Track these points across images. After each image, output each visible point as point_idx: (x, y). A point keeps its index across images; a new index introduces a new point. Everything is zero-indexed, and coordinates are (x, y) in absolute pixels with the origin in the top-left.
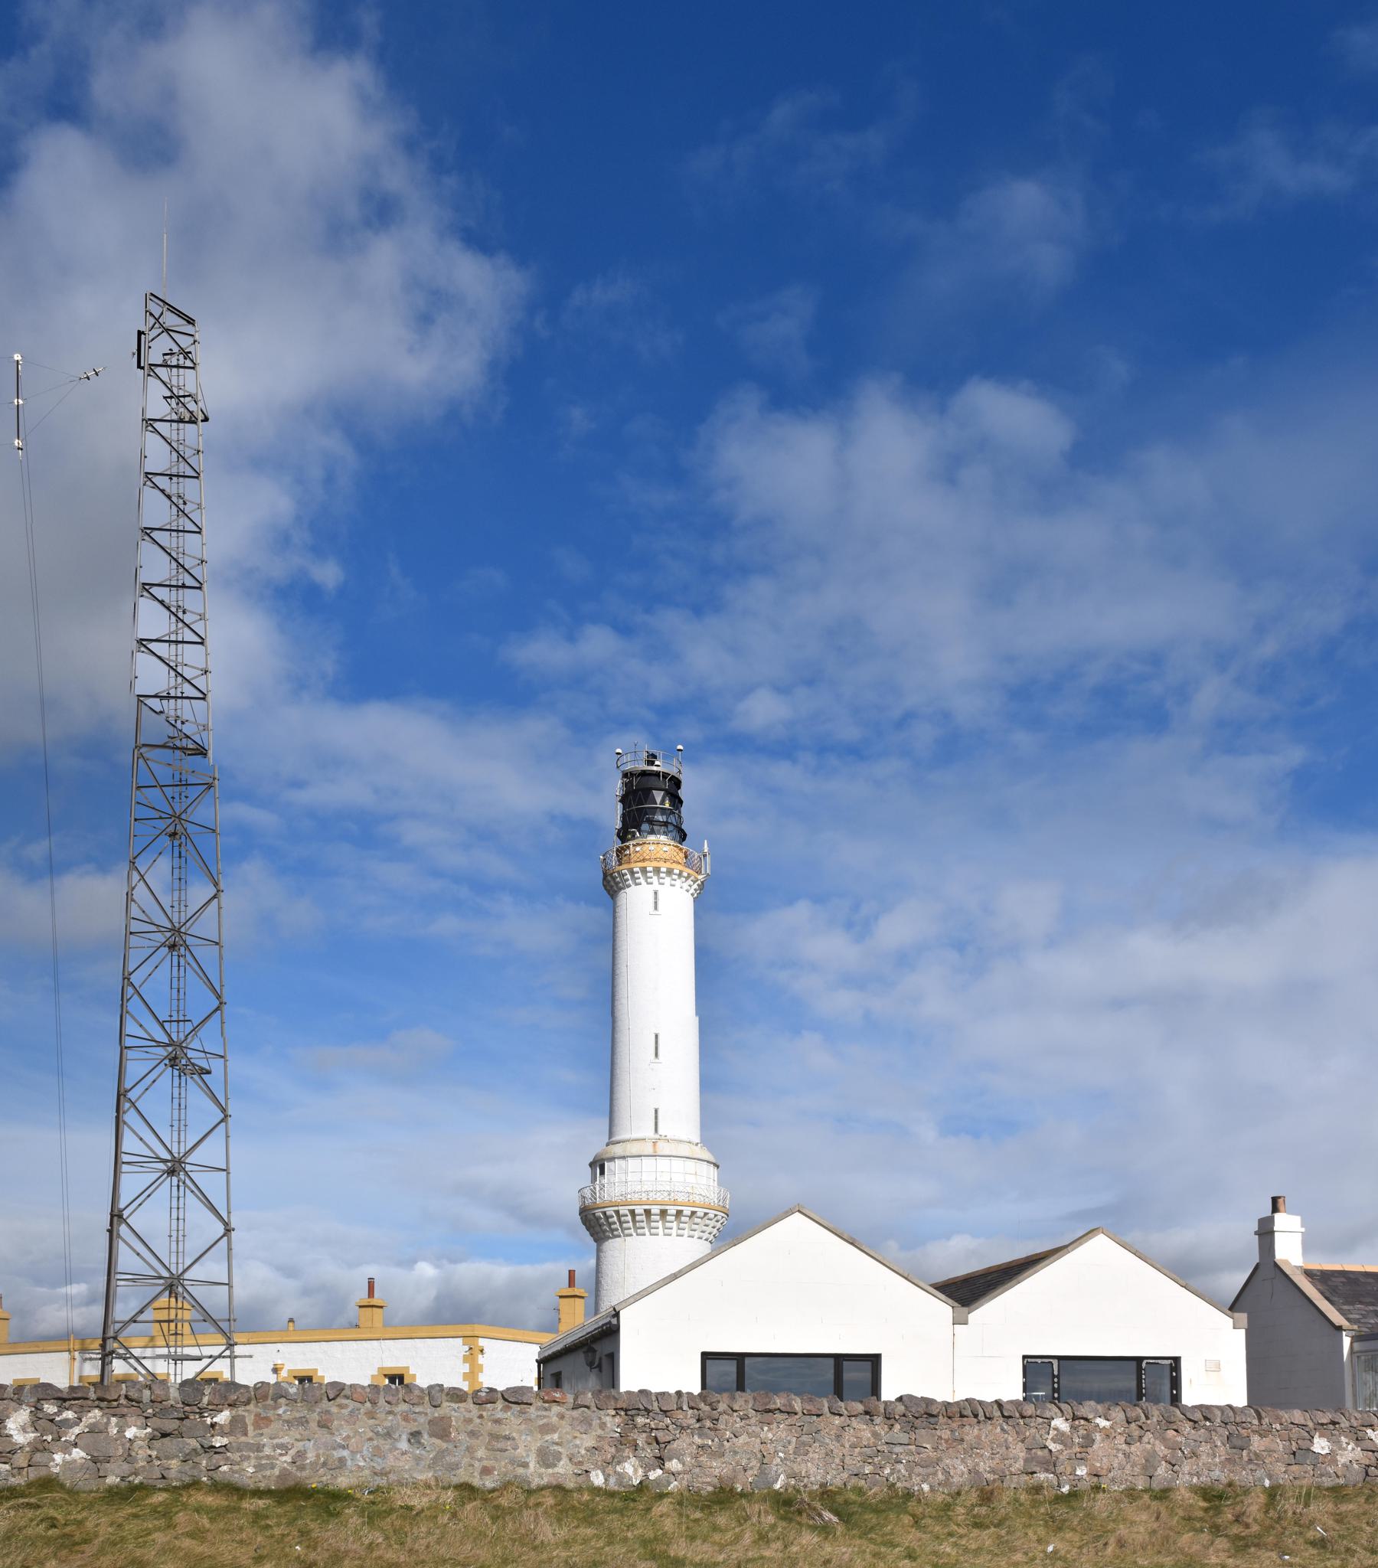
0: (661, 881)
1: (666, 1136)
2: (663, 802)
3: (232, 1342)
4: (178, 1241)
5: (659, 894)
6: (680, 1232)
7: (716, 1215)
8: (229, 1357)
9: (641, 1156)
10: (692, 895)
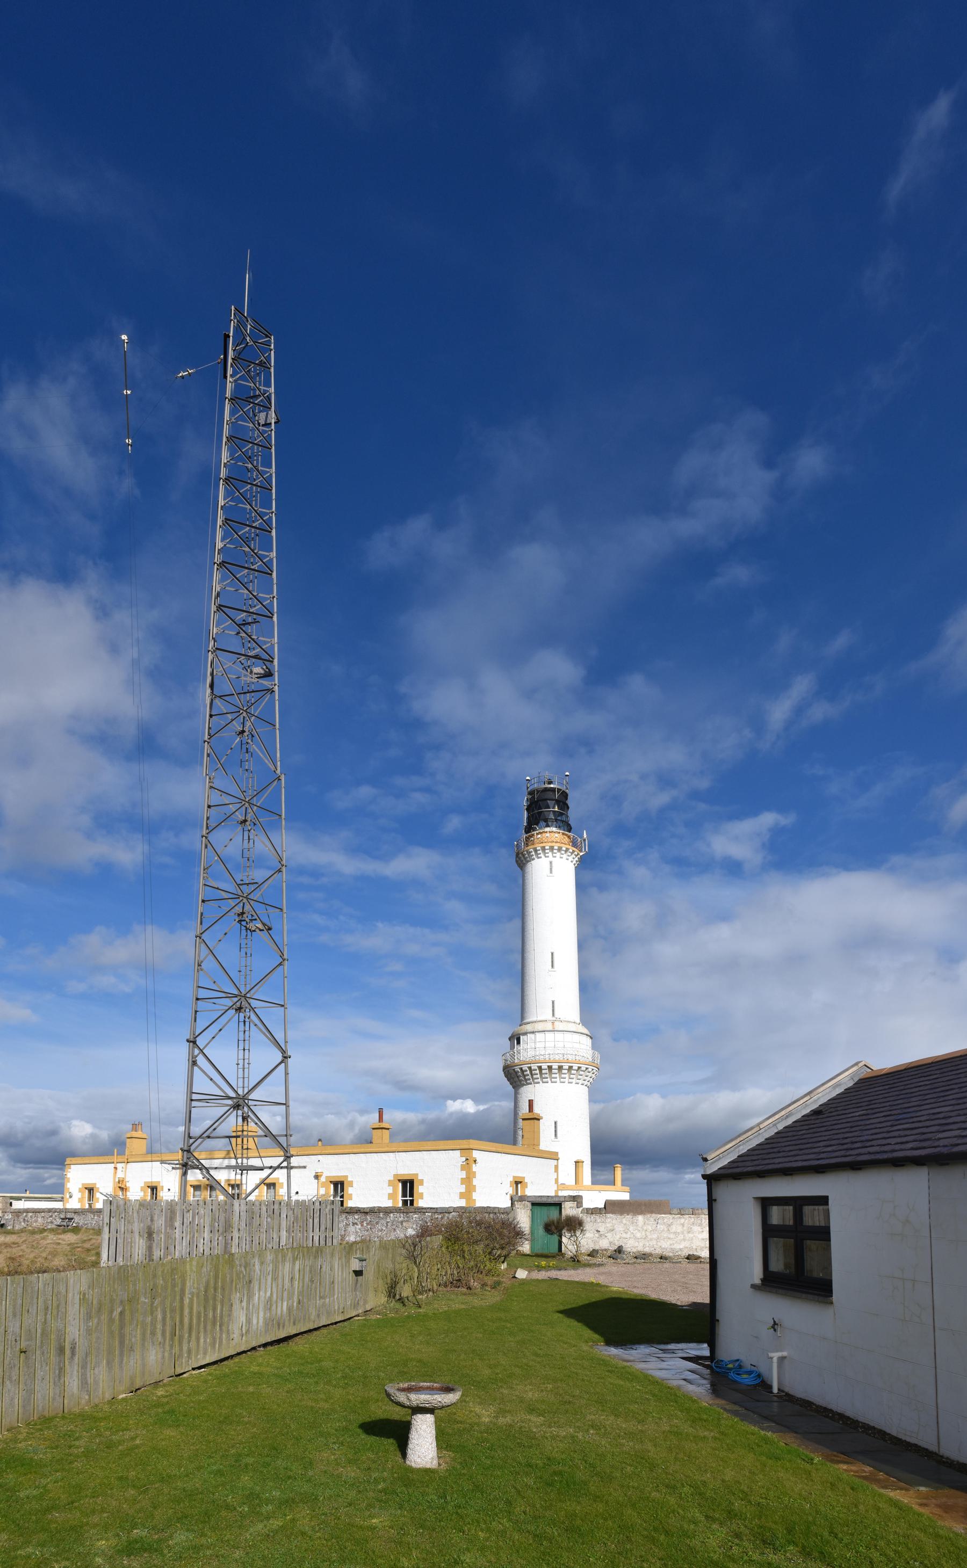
0: (554, 855)
2: (554, 808)
3: (289, 1155)
4: (244, 1069)
5: (554, 864)
6: (570, 1080)
7: (593, 1070)
8: (286, 1167)
9: (544, 1031)
10: (575, 864)
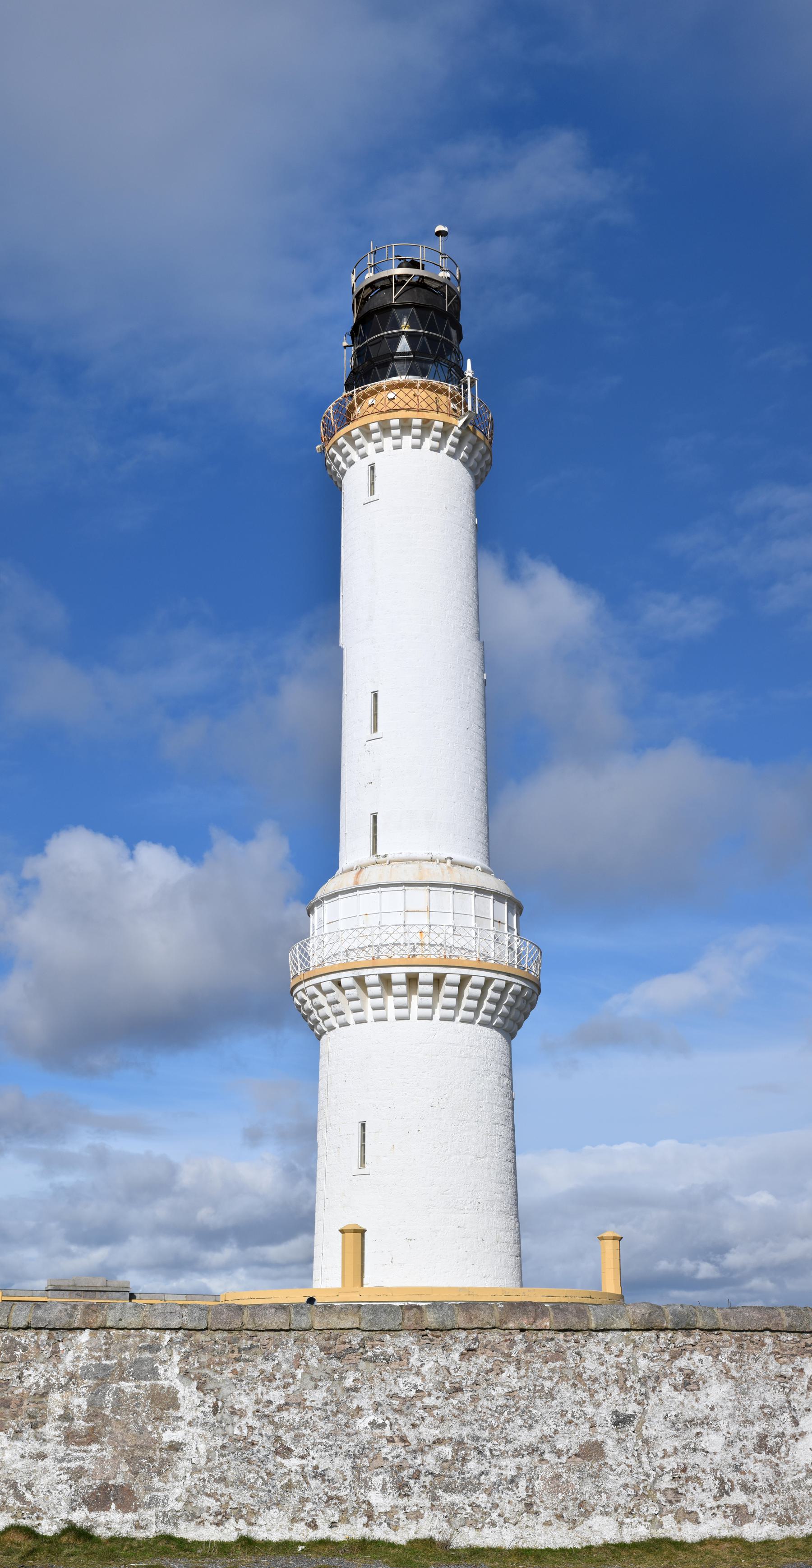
1: (386, 856)
